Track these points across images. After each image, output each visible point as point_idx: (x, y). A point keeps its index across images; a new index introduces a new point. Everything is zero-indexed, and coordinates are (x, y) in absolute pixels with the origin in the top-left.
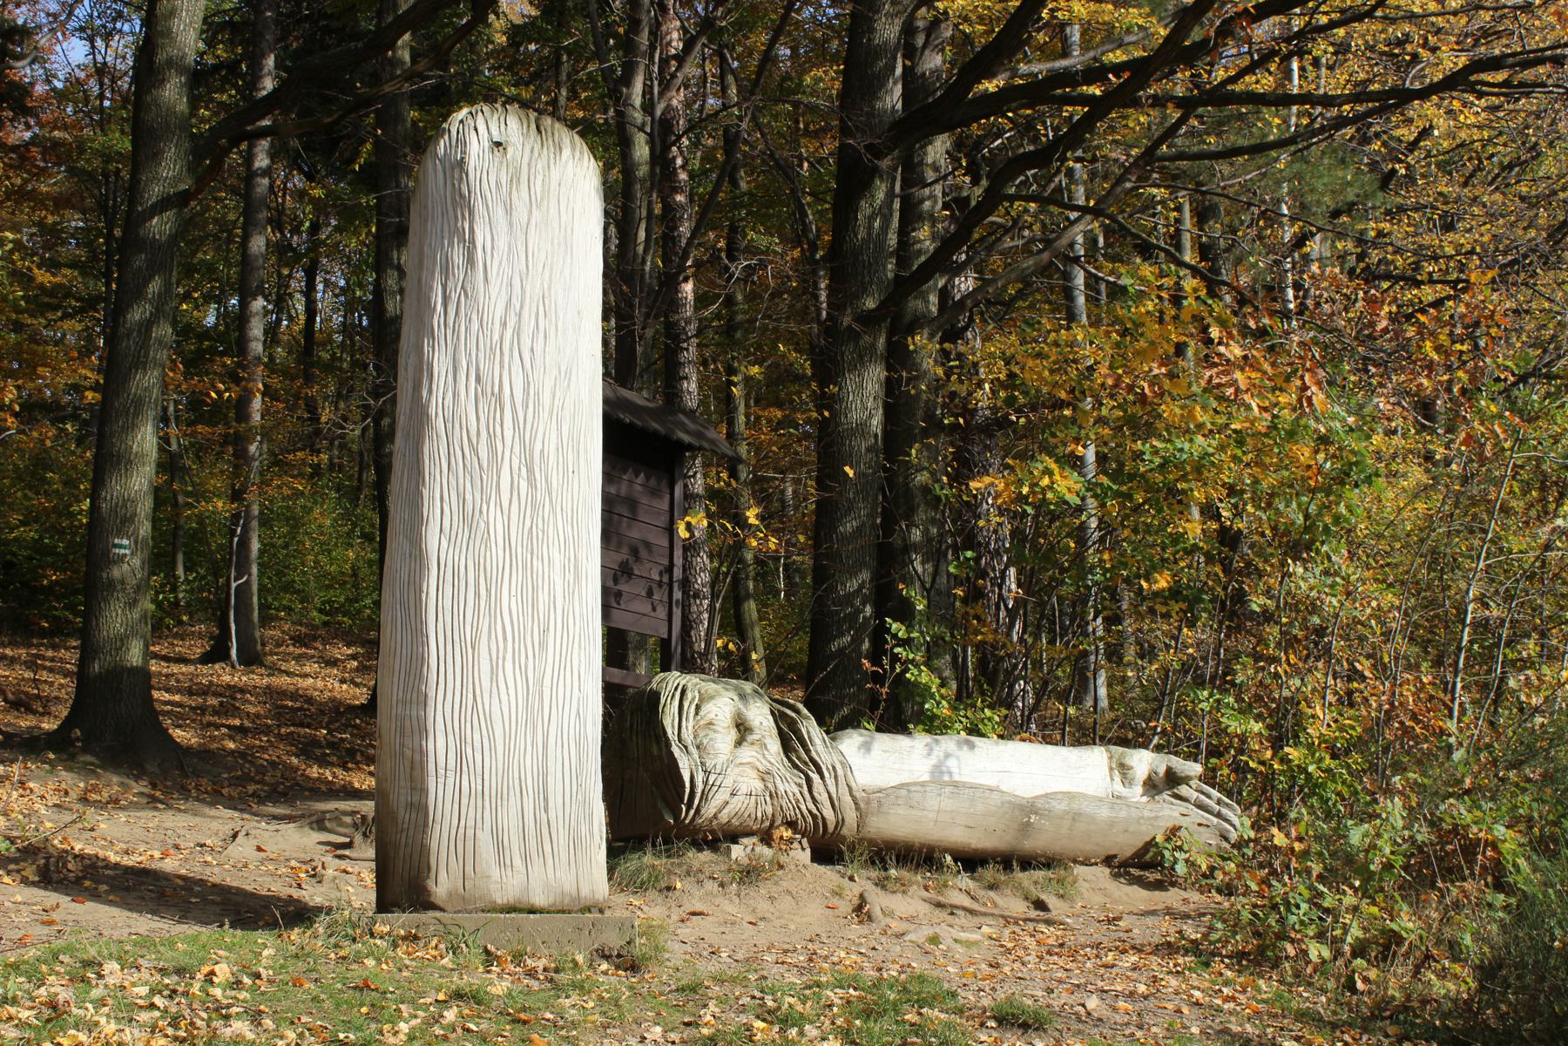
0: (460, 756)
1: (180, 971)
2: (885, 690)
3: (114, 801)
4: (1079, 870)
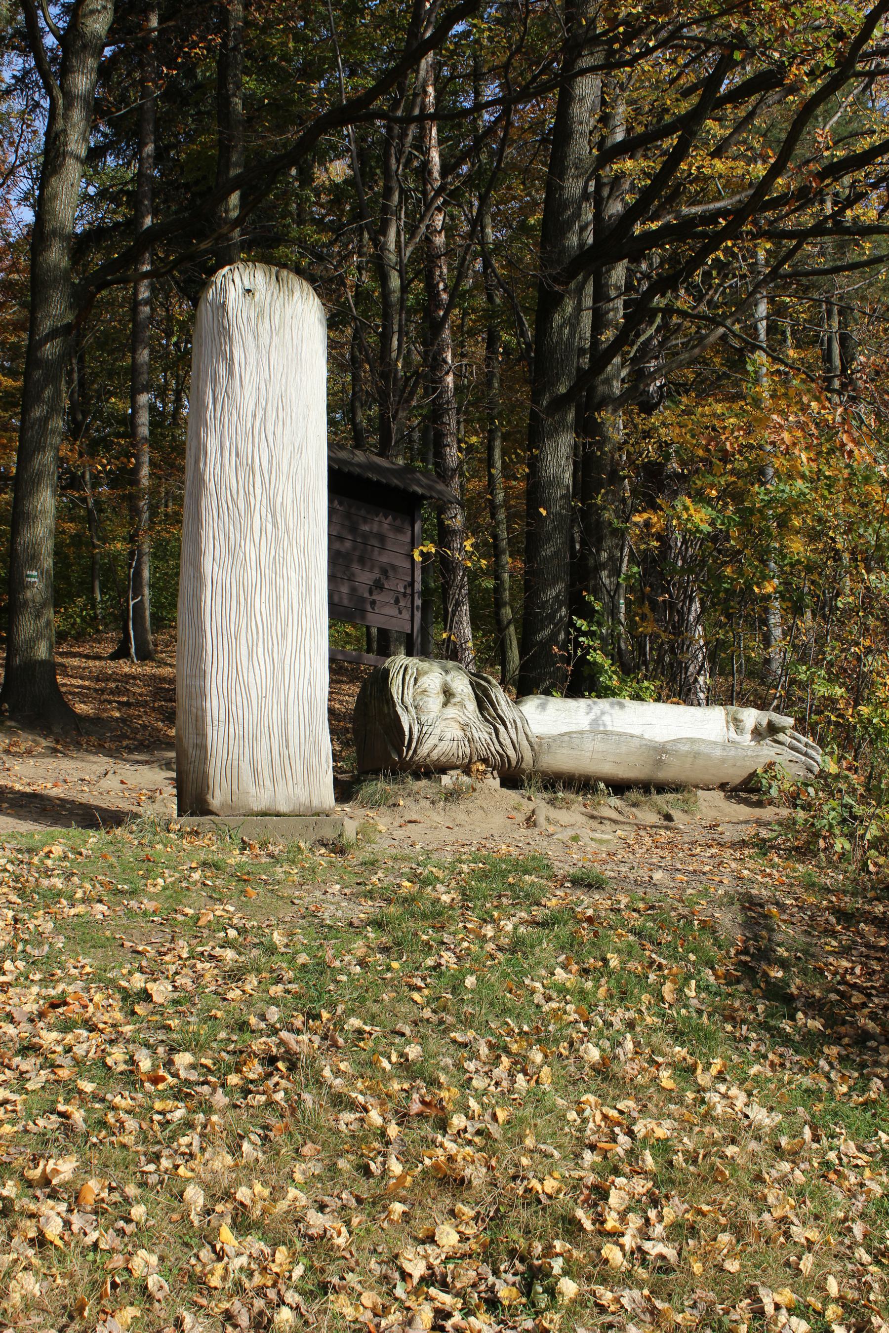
0: (228, 712)
1: (30, 851)
2: (570, 668)
3: (29, 753)
4: (700, 793)
